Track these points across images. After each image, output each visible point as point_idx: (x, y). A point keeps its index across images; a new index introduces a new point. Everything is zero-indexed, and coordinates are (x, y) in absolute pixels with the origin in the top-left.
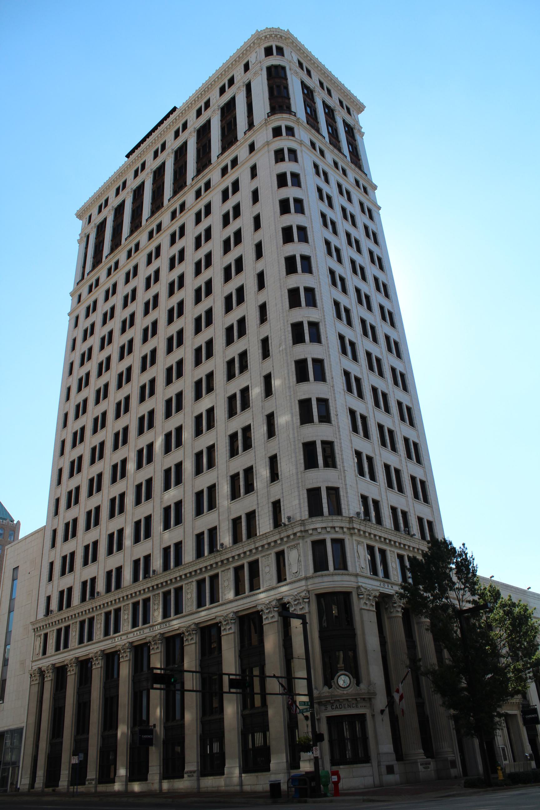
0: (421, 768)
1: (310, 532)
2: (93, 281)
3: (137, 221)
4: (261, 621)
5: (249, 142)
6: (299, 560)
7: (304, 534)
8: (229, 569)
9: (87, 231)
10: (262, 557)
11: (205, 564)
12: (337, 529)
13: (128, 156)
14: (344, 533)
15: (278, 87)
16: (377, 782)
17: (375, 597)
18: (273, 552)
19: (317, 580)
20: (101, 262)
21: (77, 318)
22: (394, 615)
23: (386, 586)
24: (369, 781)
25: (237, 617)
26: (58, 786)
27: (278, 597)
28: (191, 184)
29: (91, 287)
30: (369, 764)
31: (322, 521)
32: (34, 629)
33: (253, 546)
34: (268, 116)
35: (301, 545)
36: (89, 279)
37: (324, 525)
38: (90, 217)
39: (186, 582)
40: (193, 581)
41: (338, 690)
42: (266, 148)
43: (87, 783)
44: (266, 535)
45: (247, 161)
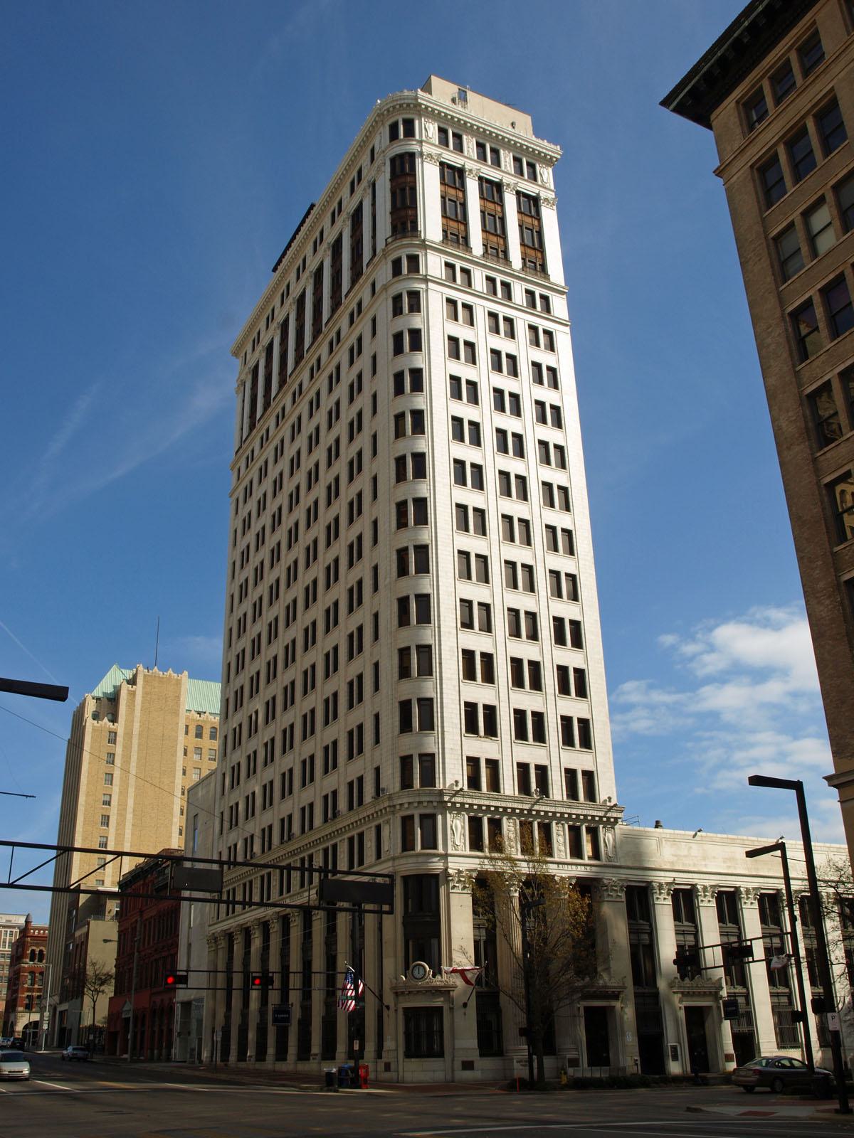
2: (354, 305)
8: (371, 827)
9: (243, 377)
13: (275, 270)
16: (449, 1077)
19: (403, 861)
20: (341, 304)
24: (440, 1076)
28: (384, 250)
29: (352, 315)
30: (442, 1059)
36: (350, 303)
38: (373, 159)
39: (340, 839)
43: (311, 1058)
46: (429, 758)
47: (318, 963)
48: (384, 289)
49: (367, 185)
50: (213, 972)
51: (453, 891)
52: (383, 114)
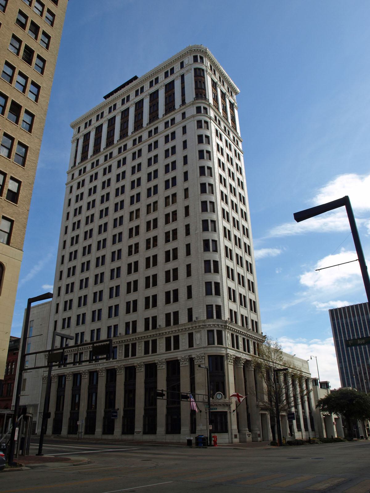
0: (247, 436)
1: (207, 326)
3: (110, 139)
4: (179, 365)
5: (183, 111)
6: (201, 338)
7: (203, 327)
10: (181, 334)
11: (150, 334)
12: (220, 326)
13: (106, 97)
14: (219, 327)
15: (200, 82)
17: (233, 358)
18: (187, 333)
21: (71, 187)
22: (239, 366)
23: (238, 353)
25: (166, 361)
26: (61, 434)
27: (189, 354)
31: (213, 322)
32: (45, 355)
33: (177, 329)
34: (194, 100)
35: (202, 331)
37: (214, 323)
40: (142, 341)
41: (217, 400)
42: (192, 119)
44: (184, 325)
45: (180, 123)
46: (210, 307)
47: (120, 403)
48: (193, 117)
49: (179, 75)
50: (205, 395)
51: (159, 368)
52: (192, 51)
